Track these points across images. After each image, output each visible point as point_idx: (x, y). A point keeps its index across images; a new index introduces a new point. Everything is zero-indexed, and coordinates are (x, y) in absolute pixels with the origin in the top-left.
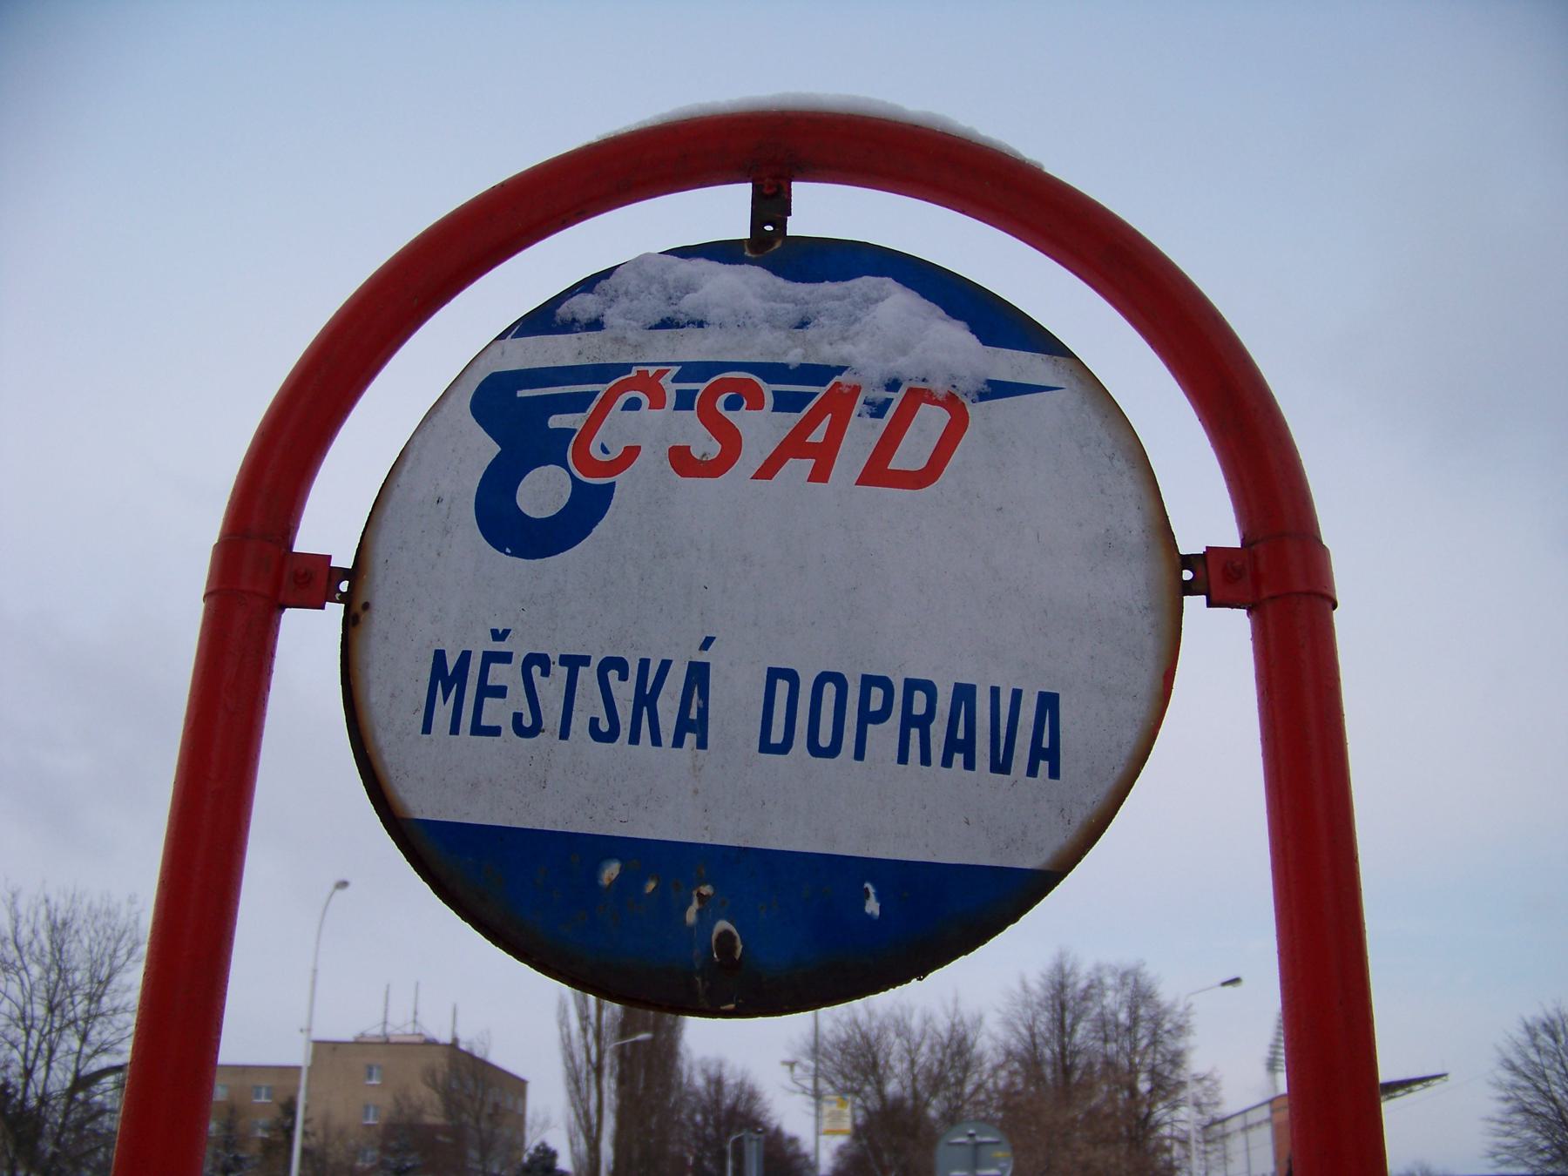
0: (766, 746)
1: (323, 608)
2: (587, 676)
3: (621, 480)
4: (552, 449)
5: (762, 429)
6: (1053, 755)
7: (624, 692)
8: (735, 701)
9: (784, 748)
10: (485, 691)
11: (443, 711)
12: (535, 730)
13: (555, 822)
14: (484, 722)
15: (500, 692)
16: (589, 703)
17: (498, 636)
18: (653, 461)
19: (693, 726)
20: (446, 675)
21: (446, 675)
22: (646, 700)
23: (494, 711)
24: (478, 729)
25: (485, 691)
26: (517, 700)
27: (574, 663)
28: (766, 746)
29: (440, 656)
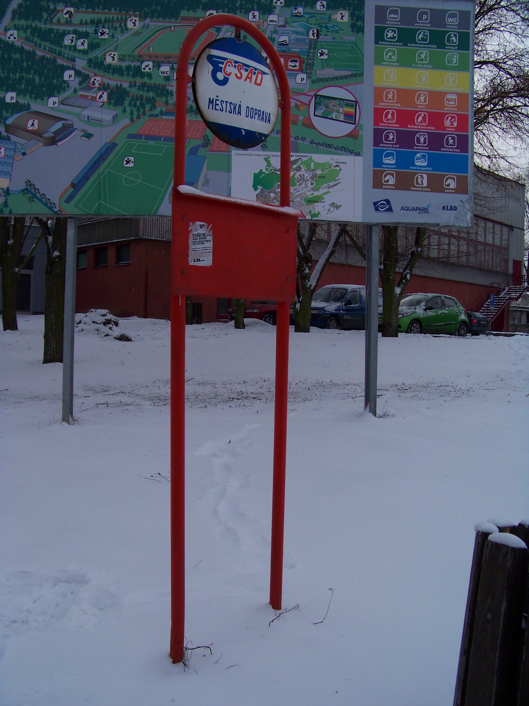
0: (246, 116)
1: (520, 524)
2: (228, 104)
3: (229, 77)
4: (220, 70)
5: (245, 74)
6: (269, 120)
7: (232, 107)
8: (243, 110)
9: (248, 117)
10: (216, 104)
11: (211, 106)
12: (222, 111)
13: (278, 162)
14: (353, 122)
15: (218, 105)
16: (228, 108)
17: (217, 97)
18: (233, 75)
19: (239, 113)
20: (211, 101)
21: (211, 101)
22: (235, 108)
23: (217, 107)
24: (215, 109)
25: (216, 104)
26: (220, 106)
27: (227, 102)
28: (246, 116)
29: (210, 98)
